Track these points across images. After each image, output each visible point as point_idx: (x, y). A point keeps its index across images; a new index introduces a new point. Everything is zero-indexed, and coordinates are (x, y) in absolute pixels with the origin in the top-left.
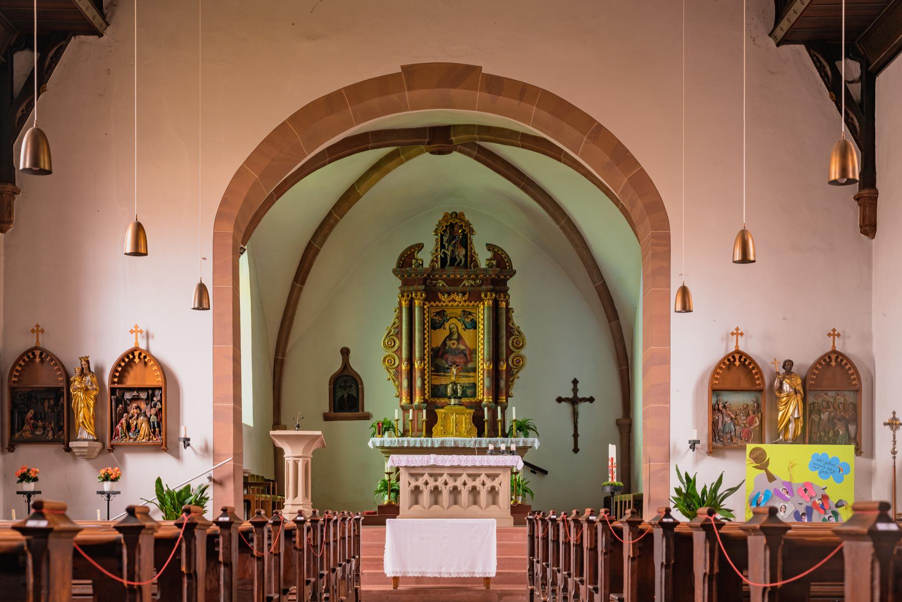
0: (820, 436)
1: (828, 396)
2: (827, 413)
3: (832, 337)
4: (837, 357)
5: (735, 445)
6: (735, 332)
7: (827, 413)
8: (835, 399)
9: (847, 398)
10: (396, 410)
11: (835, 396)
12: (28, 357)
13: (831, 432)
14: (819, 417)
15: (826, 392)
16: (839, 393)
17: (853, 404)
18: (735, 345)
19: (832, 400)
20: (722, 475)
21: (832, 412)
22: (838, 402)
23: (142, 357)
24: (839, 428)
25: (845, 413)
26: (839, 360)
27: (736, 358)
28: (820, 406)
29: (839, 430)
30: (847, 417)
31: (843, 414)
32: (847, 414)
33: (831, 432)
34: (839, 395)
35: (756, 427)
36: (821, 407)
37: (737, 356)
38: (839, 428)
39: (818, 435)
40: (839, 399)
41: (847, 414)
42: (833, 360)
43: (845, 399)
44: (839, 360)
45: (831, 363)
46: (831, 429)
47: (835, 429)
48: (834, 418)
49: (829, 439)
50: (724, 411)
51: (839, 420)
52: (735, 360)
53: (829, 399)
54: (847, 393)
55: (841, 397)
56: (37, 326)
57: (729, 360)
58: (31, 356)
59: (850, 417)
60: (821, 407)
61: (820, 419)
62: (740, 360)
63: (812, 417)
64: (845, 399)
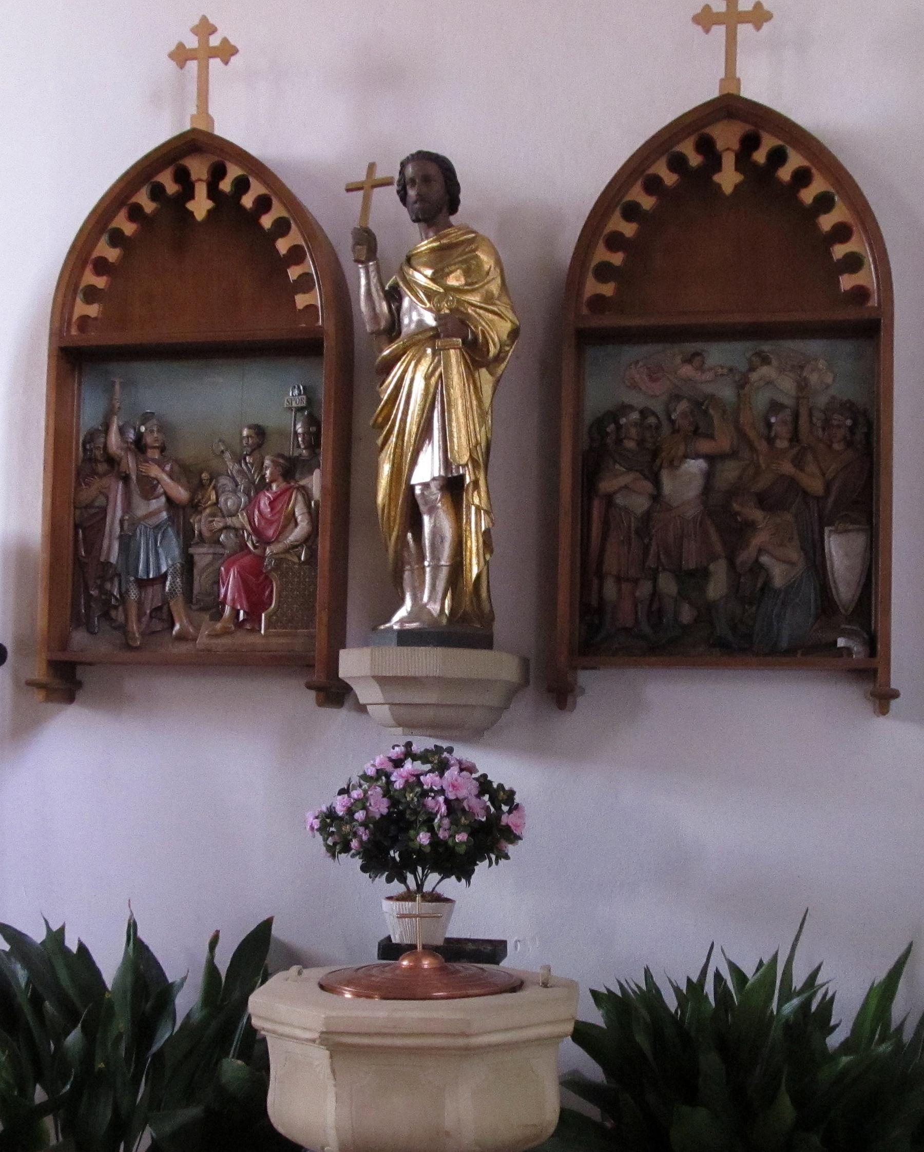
0: (655, 594)
1: (701, 368)
2: (695, 466)
3: (719, 31)
4: (750, 143)
5: (183, 648)
6: (192, 42)
7: (695, 466)
8: (742, 384)
9: (814, 378)
10: (418, 867)
11: (743, 366)
12: (157, 192)
13: (719, 571)
14: (648, 486)
15: (691, 347)
16: (766, 347)
17: (849, 408)
18: (722, 75)
19: (727, 393)
20: (777, 953)
21: (723, 457)
22: (761, 400)
23: (226, 186)
24: (760, 551)
25: (798, 463)
26: (760, 156)
27: (720, 145)
28: (658, 427)
29: (765, 559)
30: (815, 485)
31: (787, 468)
32: (812, 468)
33: (719, 571)
34: (766, 361)
35: (294, 547)
36: (666, 429)
37: (198, 169)
38: (760, 551)
39: (645, 589)
40: (769, 383)
41: (812, 468)
42: (728, 161)
43: (803, 385)
44: (760, 156)
45: (717, 178)
46: (714, 558)
47: (739, 561)
48: (734, 492)
49: (706, 613)
50: (130, 463)
51: (763, 501)
52: (713, 161)
53: (709, 389)
54: (814, 347)
55: (781, 370)
56: (205, 28)
57: (678, 163)
58: (695, 160)
59: (828, 486)
60: (666, 429)
61: (657, 497)
62: (213, 192)
63: (606, 485)
64: (803, 385)
